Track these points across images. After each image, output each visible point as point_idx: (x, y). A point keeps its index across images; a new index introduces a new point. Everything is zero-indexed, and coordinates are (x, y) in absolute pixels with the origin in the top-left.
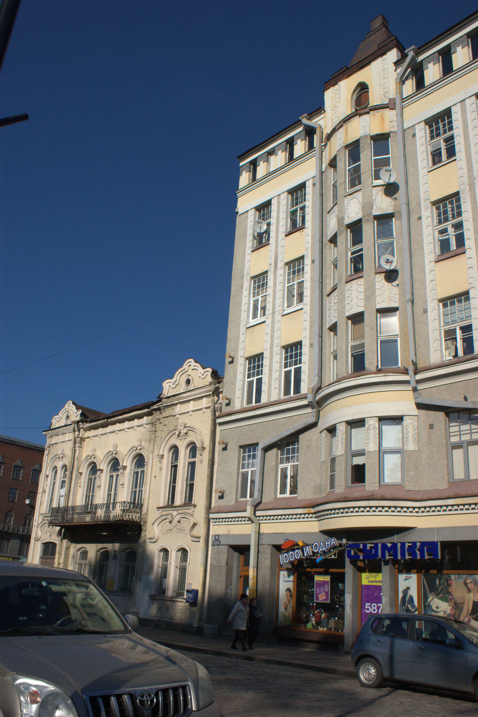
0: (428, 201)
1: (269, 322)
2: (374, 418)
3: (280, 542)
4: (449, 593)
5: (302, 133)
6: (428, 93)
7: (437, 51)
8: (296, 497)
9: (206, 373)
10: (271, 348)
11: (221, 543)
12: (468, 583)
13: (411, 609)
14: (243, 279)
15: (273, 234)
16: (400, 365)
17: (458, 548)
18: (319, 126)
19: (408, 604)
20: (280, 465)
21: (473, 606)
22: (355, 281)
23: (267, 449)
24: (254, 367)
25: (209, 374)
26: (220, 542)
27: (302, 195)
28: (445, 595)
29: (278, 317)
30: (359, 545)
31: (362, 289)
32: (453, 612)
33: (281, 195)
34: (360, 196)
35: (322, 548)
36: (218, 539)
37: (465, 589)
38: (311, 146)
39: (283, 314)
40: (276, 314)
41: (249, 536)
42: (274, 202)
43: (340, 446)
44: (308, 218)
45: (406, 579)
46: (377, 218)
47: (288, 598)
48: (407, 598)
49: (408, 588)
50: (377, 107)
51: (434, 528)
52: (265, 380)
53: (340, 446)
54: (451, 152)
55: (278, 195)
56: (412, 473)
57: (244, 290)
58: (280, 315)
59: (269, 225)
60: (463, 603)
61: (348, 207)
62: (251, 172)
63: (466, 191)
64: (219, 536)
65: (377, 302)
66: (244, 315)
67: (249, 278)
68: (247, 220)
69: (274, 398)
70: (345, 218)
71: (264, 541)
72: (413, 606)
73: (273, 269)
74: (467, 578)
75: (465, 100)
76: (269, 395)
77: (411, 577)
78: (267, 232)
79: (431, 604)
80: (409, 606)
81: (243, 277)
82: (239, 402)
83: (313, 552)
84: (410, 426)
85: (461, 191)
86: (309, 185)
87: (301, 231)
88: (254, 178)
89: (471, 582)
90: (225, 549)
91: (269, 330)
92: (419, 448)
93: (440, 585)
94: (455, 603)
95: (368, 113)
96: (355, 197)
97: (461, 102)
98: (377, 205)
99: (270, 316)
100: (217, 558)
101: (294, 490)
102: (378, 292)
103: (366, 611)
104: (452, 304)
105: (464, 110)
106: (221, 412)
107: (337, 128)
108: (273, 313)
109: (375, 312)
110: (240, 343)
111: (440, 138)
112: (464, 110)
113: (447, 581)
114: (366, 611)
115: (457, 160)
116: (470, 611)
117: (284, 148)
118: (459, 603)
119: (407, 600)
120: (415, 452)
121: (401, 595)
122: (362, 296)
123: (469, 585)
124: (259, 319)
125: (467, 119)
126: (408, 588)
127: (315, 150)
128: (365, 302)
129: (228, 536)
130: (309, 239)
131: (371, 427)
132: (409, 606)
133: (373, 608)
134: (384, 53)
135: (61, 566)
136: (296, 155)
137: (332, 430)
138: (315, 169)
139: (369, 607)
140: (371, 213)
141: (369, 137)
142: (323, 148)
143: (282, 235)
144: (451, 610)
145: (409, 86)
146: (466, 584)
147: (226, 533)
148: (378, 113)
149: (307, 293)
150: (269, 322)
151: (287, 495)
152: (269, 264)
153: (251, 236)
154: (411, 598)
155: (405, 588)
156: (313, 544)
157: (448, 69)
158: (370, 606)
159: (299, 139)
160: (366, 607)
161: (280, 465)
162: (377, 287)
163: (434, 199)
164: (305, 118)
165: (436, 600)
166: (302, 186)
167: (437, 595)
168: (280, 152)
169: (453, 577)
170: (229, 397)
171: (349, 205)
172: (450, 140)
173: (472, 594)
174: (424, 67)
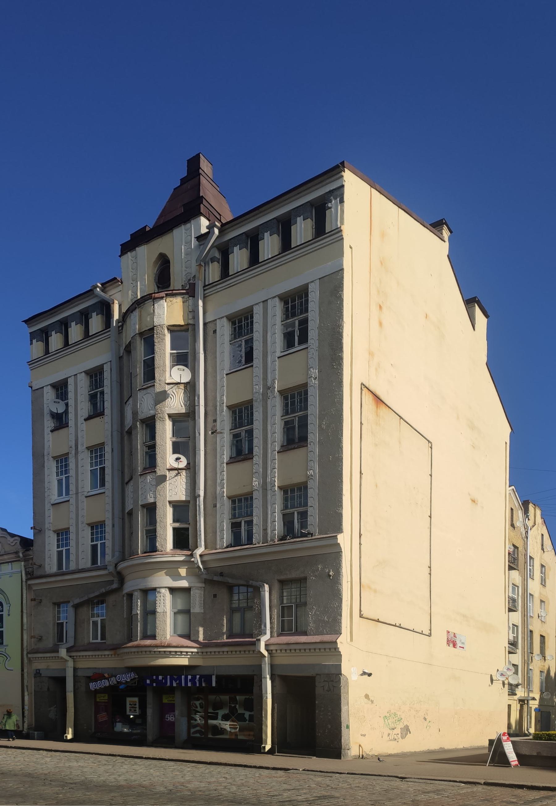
1: (73, 501)
3: (90, 674)
6: (231, 285)
7: (79, 311)
8: (105, 642)
9: (16, 541)
14: (44, 458)
15: (71, 416)
20: (91, 619)
24: (62, 539)
25: (18, 542)
27: (248, 323)
29: (81, 498)
35: (124, 678)
44: (107, 405)
52: (73, 550)
54: (304, 339)
55: (263, 302)
59: (67, 405)
70: (139, 413)
73: (73, 452)
78: (66, 412)
82: (51, 566)
83: (117, 681)
86: (107, 368)
88: (47, 351)
91: (73, 508)
96: (149, 392)
99: (74, 496)
101: (103, 637)
103: (166, 719)
106: (33, 575)
108: (77, 493)
111: (295, 318)
114: (166, 719)
124: (64, 498)
127: (109, 331)
130: (108, 426)
133: (171, 718)
136: (92, 331)
139: (169, 717)
142: (121, 328)
143: (81, 420)
149: (108, 478)
150: (73, 501)
151: (99, 640)
157: (254, 260)
158: (170, 716)
159: (53, 331)
160: (166, 717)
161: (91, 619)
168: (267, 235)
172: (304, 323)
174: (230, 250)
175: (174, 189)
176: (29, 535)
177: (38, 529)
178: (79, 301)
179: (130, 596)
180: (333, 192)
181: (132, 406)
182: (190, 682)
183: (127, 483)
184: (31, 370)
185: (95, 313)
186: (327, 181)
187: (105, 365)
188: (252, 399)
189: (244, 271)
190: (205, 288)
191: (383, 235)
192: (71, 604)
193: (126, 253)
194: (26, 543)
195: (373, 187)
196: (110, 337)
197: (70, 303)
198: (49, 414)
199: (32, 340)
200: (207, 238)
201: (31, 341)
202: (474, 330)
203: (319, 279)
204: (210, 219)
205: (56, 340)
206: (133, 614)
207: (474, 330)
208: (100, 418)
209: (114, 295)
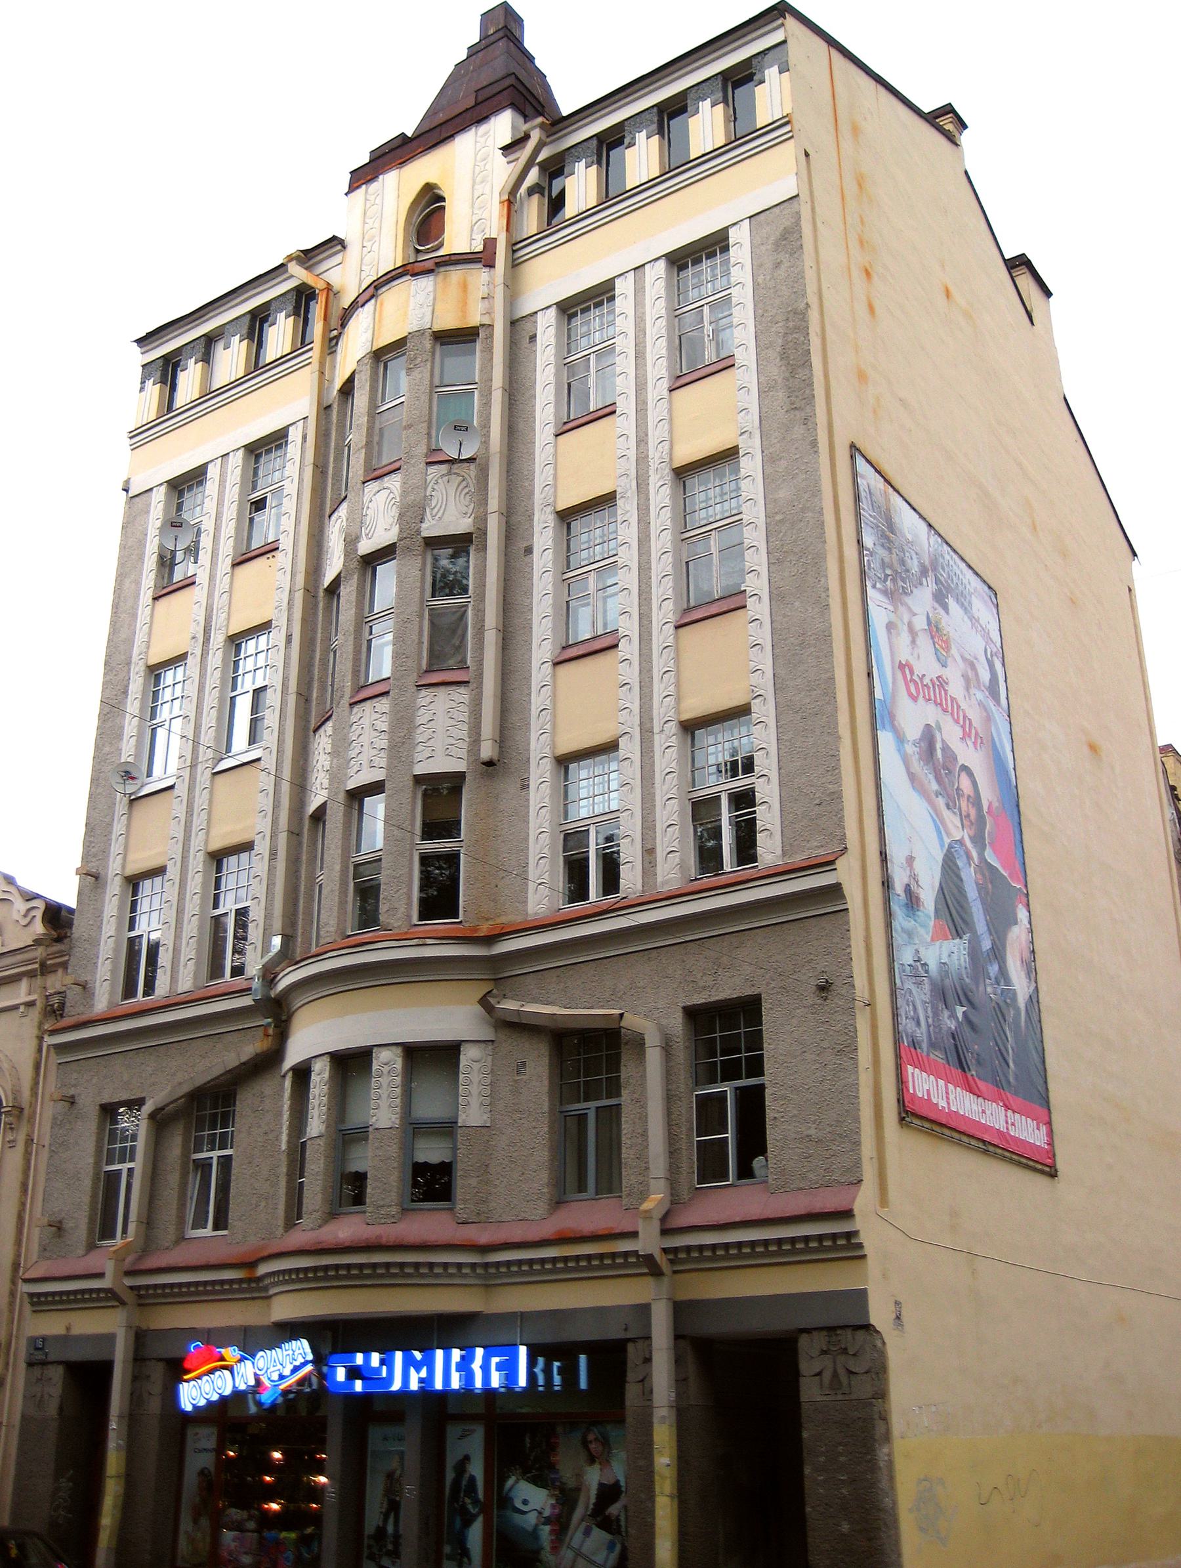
0: (549, 509)
2: (394, 1048)
5: (289, 296)
10: (185, 858)
12: (591, 1442)
17: (583, 1358)
18: (325, 286)
19: (465, 1496)
21: (598, 1496)
22: (368, 704)
25: (39, 914)
32: (557, 1511)
33: (155, 489)
34: (398, 485)
38: (302, 340)
39: (215, 771)
40: (200, 768)
41: (110, 1338)
42: (213, 472)
43: (384, 1103)
46: (432, 543)
48: (464, 1483)
50: (453, 258)
51: (515, 1313)
53: (384, 1103)
56: (473, 1182)
58: (208, 773)
62: (299, 316)
63: (628, 494)
67: (143, 668)
68: (148, 512)
69: (186, 983)
72: (476, 1502)
73: (198, 652)
75: (643, 265)
76: (174, 979)
77: (473, 1431)
79: (512, 1494)
80: (468, 1501)
81: (129, 664)
85: (619, 490)
86: (295, 435)
89: (596, 1439)
90: (57, 1374)
91: (180, 810)
94: (562, 1490)
95: (430, 271)
96: (385, 485)
97: (635, 269)
105: (639, 290)
107: (361, 300)
109: (411, 783)
110: (114, 837)
112: (639, 290)
115: (197, 584)
117: (245, 331)
118: (571, 1489)
119: (463, 1487)
120: (484, 1131)
121: (450, 1476)
123: (592, 1446)
128: (390, 758)
129: (65, 1339)
132: (468, 1501)
134: (482, 119)
135: (455, 1384)
137: (302, 1073)
138: (308, 398)
140: (418, 532)
141: (428, 334)
142: (334, 342)
144: (553, 1506)
145: (532, 214)
146: (585, 1444)
147: (62, 1331)
148: (456, 274)
152: (191, 636)
153: (155, 557)
154: (472, 1479)
155: (461, 1457)
164: (294, 262)
166: (277, 439)
168: (641, 137)
170: (82, 978)
175: (456, 66)
176: (67, 895)
177: (92, 877)
178: (763, 26)
179: (302, 1073)
180: (765, 54)
181: (344, 523)
182: (458, 1374)
183: (316, 730)
184: (132, 450)
185: (644, 133)
186: (210, 315)
187: (731, 232)
188: (615, 491)
189: (651, 183)
190: (514, 248)
191: (856, 130)
192: (148, 1108)
193: (358, 187)
194: (56, 916)
195: (832, 46)
196: (310, 363)
197: (235, 295)
198: (156, 554)
199: (145, 382)
200: (524, 147)
201: (143, 382)
202: (1032, 323)
203: (750, 217)
204: (527, 113)
205: (189, 381)
206: (308, 1136)
207: (1032, 323)
208: (268, 558)
209: (325, 274)
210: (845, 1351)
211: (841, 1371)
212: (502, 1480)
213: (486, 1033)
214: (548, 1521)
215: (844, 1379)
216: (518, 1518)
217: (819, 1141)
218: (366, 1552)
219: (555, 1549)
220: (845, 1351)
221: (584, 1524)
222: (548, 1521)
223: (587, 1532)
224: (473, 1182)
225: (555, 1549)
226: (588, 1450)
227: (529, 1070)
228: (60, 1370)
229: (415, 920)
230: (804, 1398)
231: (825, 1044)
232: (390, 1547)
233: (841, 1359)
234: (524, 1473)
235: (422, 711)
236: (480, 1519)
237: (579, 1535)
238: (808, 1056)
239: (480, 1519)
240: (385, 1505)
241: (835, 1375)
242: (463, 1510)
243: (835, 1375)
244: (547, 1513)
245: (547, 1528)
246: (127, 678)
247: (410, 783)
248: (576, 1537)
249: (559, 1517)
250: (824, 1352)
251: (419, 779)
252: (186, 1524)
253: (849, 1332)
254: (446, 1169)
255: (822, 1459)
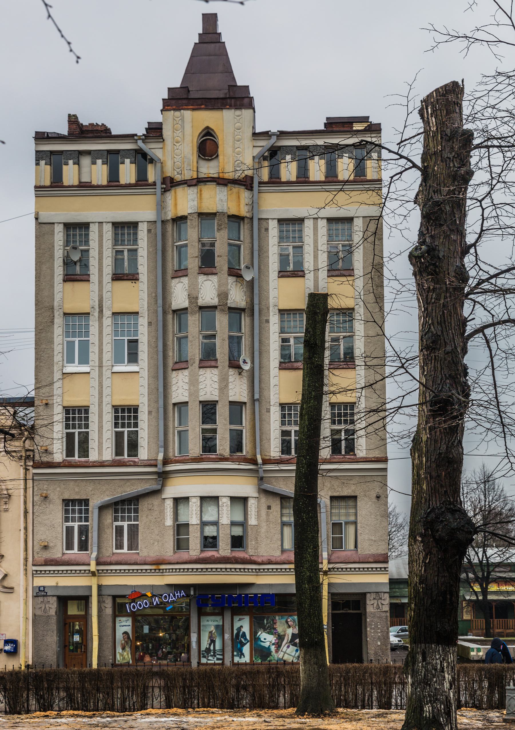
0: (276, 308)
4: (275, 629)
11: (48, 594)
13: (244, 641)
16: (244, 453)
21: (292, 637)
23: (102, 508)
26: (46, 593)
28: (271, 630)
30: (207, 595)
31: (216, 378)
32: (277, 641)
35: (172, 598)
36: (44, 590)
37: (286, 626)
40: (104, 369)
41: (90, 588)
45: (240, 620)
47: (126, 640)
48: (241, 634)
49: (242, 627)
53: (194, 516)
56: (253, 543)
57: (56, 326)
60: (285, 635)
61: (202, 287)
64: (44, 587)
65: (230, 394)
66: (57, 358)
71: (105, 592)
73: (96, 314)
74: (288, 618)
80: (242, 639)
84: (253, 505)
87: (133, 281)
92: (259, 523)
93: (267, 623)
94: (279, 635)
96: (210, 279)
98: (232, 296)
100: (43, 608)
102: (231, 386)
104: (123, 228)
113: (273, 620)
116: (289, 640)
121: (235, 632)
122: (216, 386)
125: (317, 239)
126: (242, 627)
129: (57, 587)
131: (225, 505)
132: (242, 639)
140: (227, 304)
144: (276, 640)
146: (287, 622)
152: (91, 306)
154: (244, 633)
156: (162, 595)
162: (230, 381)
163: (281, 307)
165: (264, 634)
167: (265, 630)
169: (277, 618)
171: (175, 288)
173: (291, 629)
210: (381, 599)
211: (380, 604)
212: (256, 633)
213: (256, 495)
214: (273, 644)
215: (381, 606)
216: (262, 644)
217: (375, 541)
218: (202, 656)
219: (277, 652)
220: (381, 599)
221: (287, 645)
222: (273, 644)
223: (288, 647)
224: (253, 543)
225: (277, 652)
226: (288, 624)
227: (273, 508)
228: (55, 599)
229: (201, 453)
230: (368, 610)
231: (378, 514)
232: (212, 654)
233: (380, 601)
234: (264, 631)
235: (174, 379)
236: (248, 644)
237: (285, 648)
238: (372, 516)
239: (248, 644)
240: (209, 641)
241: (378, 604)
242: (241, 642)
243: (378, 604)
244: (273, 642)
245: (274, 646)
246: (52, 315)
247: (198, 402)
248: (284, 648)
249: (278, 643)
250: (374, 599)
251: (200, 402)
252: (119, 650)
253: (382, 594)
254: (215, 538)
255: (373, 626)
